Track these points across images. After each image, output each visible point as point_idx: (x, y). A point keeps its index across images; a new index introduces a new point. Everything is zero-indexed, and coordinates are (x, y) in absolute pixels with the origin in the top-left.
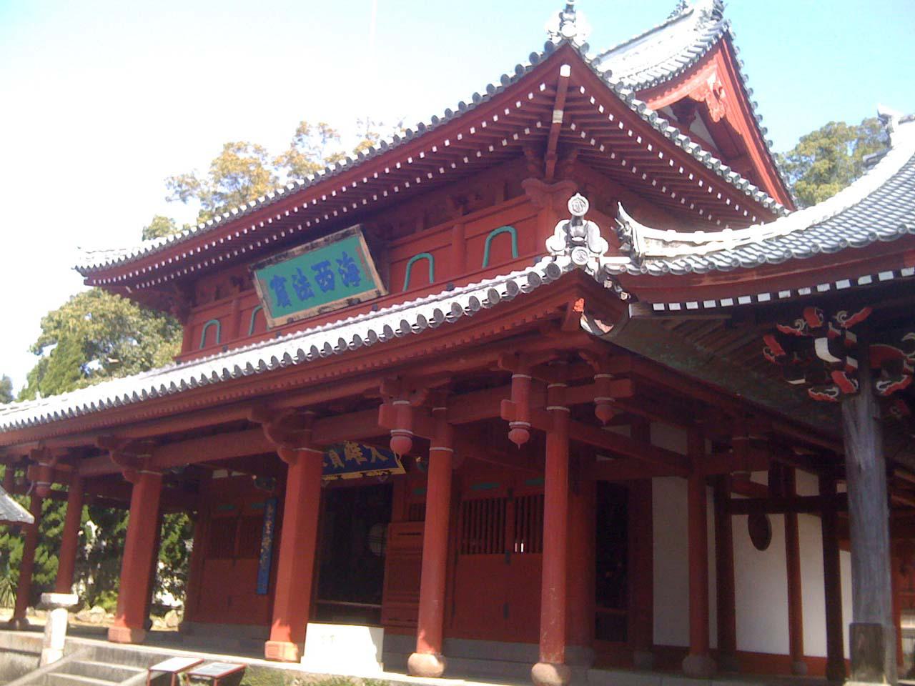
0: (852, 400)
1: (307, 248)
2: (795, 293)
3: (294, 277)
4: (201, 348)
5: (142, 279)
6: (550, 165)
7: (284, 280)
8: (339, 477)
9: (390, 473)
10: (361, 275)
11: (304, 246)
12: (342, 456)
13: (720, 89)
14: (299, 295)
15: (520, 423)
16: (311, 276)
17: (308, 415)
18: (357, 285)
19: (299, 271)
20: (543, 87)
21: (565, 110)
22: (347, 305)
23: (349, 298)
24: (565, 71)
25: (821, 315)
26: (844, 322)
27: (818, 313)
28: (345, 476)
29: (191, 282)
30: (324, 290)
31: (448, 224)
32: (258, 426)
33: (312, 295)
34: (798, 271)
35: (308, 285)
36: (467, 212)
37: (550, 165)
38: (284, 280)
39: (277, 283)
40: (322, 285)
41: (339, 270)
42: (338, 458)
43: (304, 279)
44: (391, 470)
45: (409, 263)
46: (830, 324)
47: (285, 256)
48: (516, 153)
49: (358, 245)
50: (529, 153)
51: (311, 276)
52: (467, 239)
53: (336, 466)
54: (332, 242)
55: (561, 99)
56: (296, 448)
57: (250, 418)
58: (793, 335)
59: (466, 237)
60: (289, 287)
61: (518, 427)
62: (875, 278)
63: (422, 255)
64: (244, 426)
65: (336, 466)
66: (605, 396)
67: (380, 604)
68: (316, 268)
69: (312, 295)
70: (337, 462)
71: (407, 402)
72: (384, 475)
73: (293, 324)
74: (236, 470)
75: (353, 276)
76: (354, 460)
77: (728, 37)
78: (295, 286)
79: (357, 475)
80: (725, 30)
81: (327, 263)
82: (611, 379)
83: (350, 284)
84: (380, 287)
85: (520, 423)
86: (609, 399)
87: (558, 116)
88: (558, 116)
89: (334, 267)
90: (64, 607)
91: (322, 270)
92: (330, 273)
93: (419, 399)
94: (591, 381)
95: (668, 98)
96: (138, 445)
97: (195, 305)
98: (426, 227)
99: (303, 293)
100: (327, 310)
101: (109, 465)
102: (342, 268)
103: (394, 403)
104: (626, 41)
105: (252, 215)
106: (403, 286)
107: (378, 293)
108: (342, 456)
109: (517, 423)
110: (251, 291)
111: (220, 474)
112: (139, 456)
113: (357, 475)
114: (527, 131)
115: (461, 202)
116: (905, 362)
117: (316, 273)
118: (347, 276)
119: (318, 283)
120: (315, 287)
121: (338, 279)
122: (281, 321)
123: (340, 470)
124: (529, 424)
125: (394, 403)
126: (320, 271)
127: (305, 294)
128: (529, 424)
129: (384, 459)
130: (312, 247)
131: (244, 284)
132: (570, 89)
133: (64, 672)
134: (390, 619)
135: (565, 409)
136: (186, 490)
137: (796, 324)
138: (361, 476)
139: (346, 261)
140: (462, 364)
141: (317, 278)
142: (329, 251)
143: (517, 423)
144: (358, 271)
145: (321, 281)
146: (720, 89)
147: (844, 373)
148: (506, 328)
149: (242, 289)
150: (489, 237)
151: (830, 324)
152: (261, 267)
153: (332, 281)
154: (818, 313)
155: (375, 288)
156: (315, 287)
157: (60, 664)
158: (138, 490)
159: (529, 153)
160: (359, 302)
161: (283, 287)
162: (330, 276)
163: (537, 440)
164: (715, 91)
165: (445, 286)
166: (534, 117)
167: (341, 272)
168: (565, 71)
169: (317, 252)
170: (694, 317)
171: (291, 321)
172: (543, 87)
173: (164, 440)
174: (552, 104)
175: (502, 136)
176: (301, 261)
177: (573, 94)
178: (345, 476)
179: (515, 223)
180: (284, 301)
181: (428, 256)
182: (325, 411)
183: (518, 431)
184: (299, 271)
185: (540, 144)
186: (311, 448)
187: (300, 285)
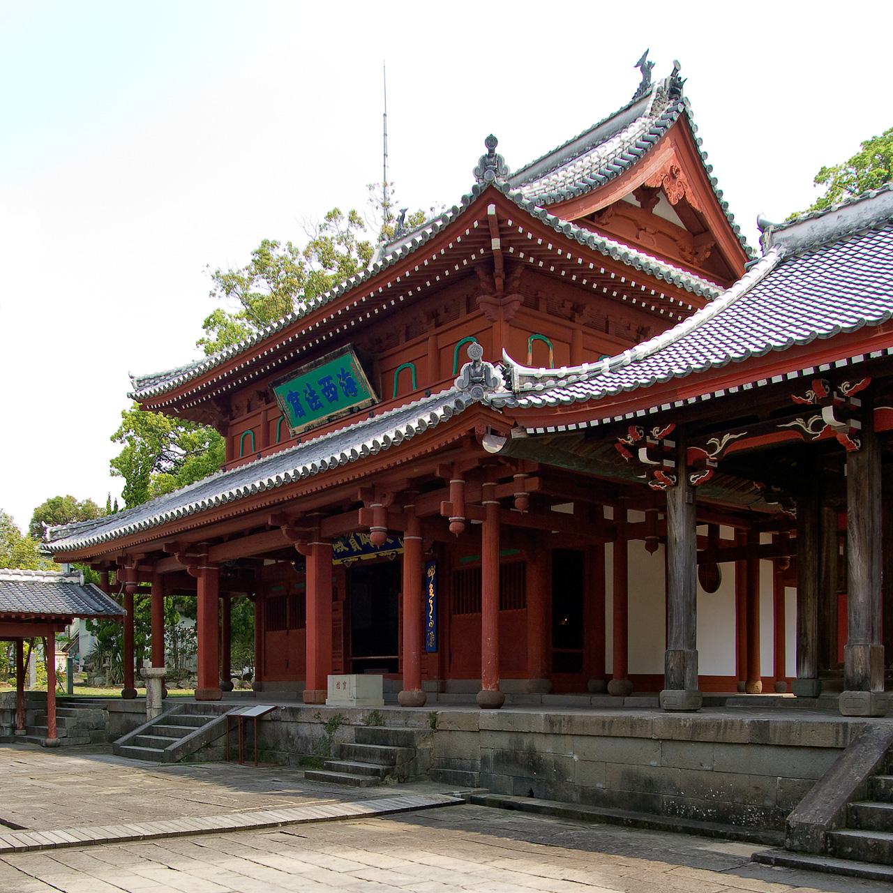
0: (673, 489)
1: (312, 365)
2: (612, 419)
4: (414, 389)
5: (185, 400)
6: (499, 282)
8: (359, 558)
9: (397, 552)
11: (309, 364)
13: (678, 170)
14: (312, 407)
15: (456, 518)
16: (318, 389)
17: (316, 515)
18: (355, 395)
19: (308, 385)
20: (476, 224)
21: (501, 237)
22: (349, 413)
23: (350, 407)
24: (491, 210)
25: (827, 387)
26: (847, 392)
27: (638, 430)
29: (224, 399)
30: (330, 400)
31: (424, 336)
33: (321, 405)
34: (613, 404)
36: (438, 325)
37: (499, 282)
38: (297, 394)
39: (293, 397)
40: (327, 397)
41: (340, 383)
43: (312, 393)
44: (397, 550)
45: (396, 373)
46: (835, 393)
47: (296, 373)
48: (469, 273)
49: (352, 363)
50: (480, 272)
51: (318, 389)
52: (440, 349)
53: (355, 550)
54: (331, 359)
55: (494, 229)
56: (309, 542)
58: (627, 444)
59: (439, 348)
60: (302, 398)
61: (455, 521)
62: (660, 408)
63: (405, 363)
64: (261, 529)
65: (355, 550)
66: (521, 492)
67: (397, 655)
68: (321, 382)
69: (321, 405)
70: (356, 547)
71: (381, 505)
72: (393, 554)
73: (309, 432)
74: (281, 559)
75: (351, 389)
77: (685, 116)
78: (307, 399)
79: (372, 556)
80: (681, 111)
82: (526, 478)
84: (374, 397)
85: (456, 518)
86: (524, 494)
87: (496, 244)
88: (496, 244)
89: (335, 381)
90: (157, 678)
92: (333, 386)
93: (387, 502)
94: (510, 479)
95: (621, 191)
96: (194, 547)
97: (232, 419)
98: (407, 340)
100: (335, 418)
101: (175, 564)
103: (371, 506)
104: (607, 116)
107: (373, 401)
109: (454, 518)
111: (268, 562)
112: (198, 556)
113: (372, 556)
114: (482, 251)
115: (434, 315)
116: (707, 460)
118: (346, 387)
119: (325, 394)
120: (322, 399)
122: (299, 429)
123: (358, 552)
124: (463, 518)
125: (371, 506)
126: (325, 385)
127: (316, 406)
128: (463, 518)
129: (347, 549)
130: (316, 365)
132: (500, 222)
135: (496, 502)
136: (237, 579)
137: (628, 438)
138: (376, 556)
139: (344, 375)
140: (416, 471)
141: (324, 391)
142: (330, 368)
143: (454, 518)
145: (327, 393)
146: (678, 170)
147: (662, 472)
148: (456, 439)
149: (268, 402)
150: (457, 347)
151: (835, 393)
152: (278, 384)
153: (335, 393)
154: (638, 430)
155: (369, 397)
156: (322, 399)
157: (159, 719)
158: (201, 583)
159: (480, 272)
160: (359, 410)
161: (298, 400)
162: (333, 389)
163: (472, 533)
164: (672, 173)
165: (424, 393)
167: (342, 385)
168: (491, 210)
169: (320, 368)
170: (564, 435)
171: (309, 429)
172: (476, 224)
173: (218, 541)
174: (500, 225)
175: (470, 251)
176: (309, 378)
177: (503, 226)
179: (475, 334)
180: (300, 412)
181: (411, 365)
183: (455, 523)
184: (308, 385)
185: (489, 261)
186: (322, 542)
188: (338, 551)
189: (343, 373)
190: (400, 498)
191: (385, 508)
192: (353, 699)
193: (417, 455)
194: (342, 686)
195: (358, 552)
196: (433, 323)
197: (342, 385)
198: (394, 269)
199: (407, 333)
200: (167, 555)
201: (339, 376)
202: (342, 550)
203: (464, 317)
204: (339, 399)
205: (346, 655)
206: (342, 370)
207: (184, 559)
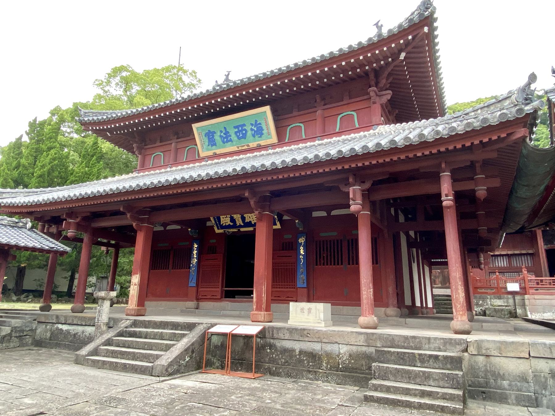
3: (221, 132)
4: (287, 141)
7: (214, 132)
10: (265, 132)
12: (243, 219)
19: (225, 128)
28: (242, 229)
30: (239, 138)
32: (123, 213)
35: (230, 136)
38: (214, 132)
39: (210, 135)
42: (240, 220)
43: (227, 133)
57: (121, 209)
65: (238, 224)
69: (231, 140)
70: (239, 222)
75: (259, 132)
76: (250, 222)
78: (221, 136)
81: (244, 125)
83: (257, 136)
91: (240, 128)
97: (146, 145)
98: (160, 142)
99: (225, 140)
102: (253, 128)
105: (167, 108)
106: (336, 127)
108: (243, 219)
110: (191, 137)
117: (236, 130)
118: (255, 131)
120: (234, 137)
121: (249, 133)
129: (231, 224)
131: (187, 135)
133: (117, 336)
134: (253, 321)
144: (263, 130)
156: (234, 137)
166: (316, 79)
167: (252, 130)
178: (242, 229)
181: (301, 125)
182: (155, 209)
184: (225, 128)
187: (224, 136)
188: (224, 225)
189: (256, 123)
190: (85, 219)
191: (77, 223)
192: (320, 321)
193: (105, 201)
194: (306, 311)
195: (241, 226)
196: (176, 137)
197: (252, 130)
198: (318, 66)
199: (161, 140)
200: (123, 213)
201: (252, 125)
202: (227, 224)
203: (158, 144)
204: (217, 144)
205: (222, 287)
206: (256, 121)
207: (133, 218)
